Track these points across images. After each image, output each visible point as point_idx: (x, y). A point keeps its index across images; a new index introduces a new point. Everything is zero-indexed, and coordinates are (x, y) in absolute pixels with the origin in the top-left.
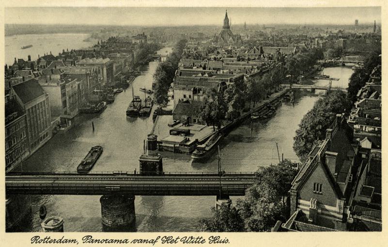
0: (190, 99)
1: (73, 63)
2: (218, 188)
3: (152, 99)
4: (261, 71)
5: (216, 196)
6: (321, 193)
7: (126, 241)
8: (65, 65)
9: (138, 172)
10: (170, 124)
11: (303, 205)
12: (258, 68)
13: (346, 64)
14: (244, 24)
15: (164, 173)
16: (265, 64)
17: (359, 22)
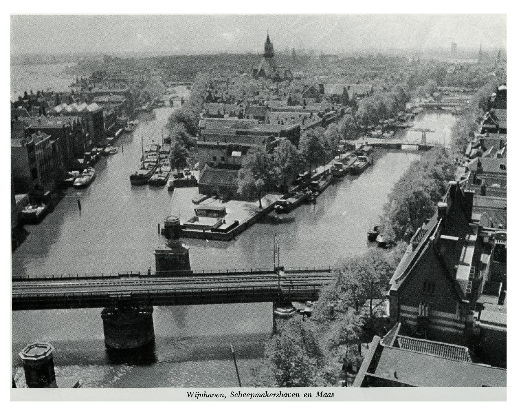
0: (223, 162)
1: (42, 112)
2: (276, 290)
3: (458, 179)
4: (324, 121)
5: (272, 303)
6: (433, 294)
7: (298, 395)
8: (31, 115)
9: (153, 272)
10: (195, 201)
11: (407, 312)
12: (320, 115)
13: (443, 108)
14: (479, 50)
15: (192, 271)
16: (329, 108)
17: (458, 46)
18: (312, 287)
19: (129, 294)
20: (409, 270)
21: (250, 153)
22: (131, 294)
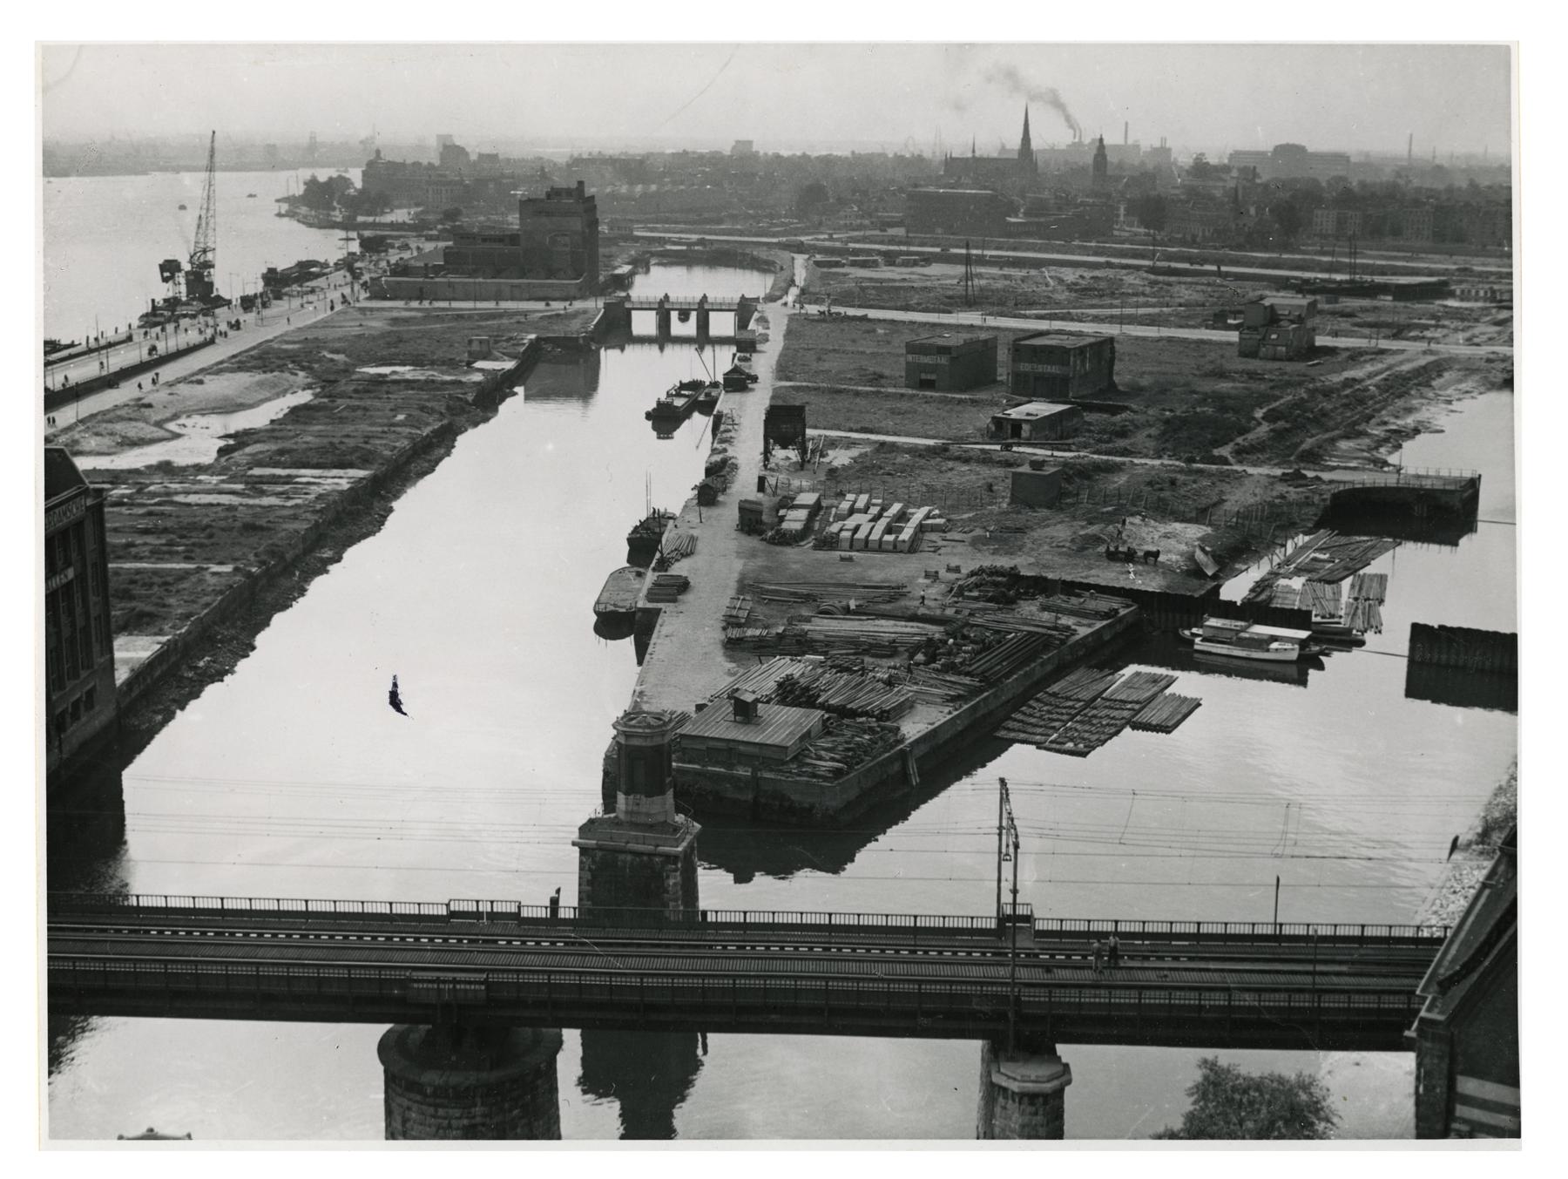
18: (1134, 993)
19: (480, 983)
20: (1492, 946)
21: (1473, 888)
22: (485, 982)
